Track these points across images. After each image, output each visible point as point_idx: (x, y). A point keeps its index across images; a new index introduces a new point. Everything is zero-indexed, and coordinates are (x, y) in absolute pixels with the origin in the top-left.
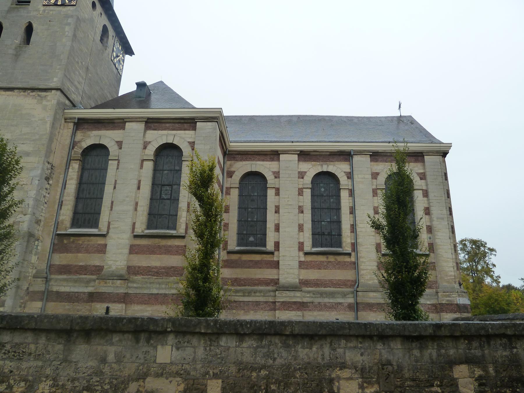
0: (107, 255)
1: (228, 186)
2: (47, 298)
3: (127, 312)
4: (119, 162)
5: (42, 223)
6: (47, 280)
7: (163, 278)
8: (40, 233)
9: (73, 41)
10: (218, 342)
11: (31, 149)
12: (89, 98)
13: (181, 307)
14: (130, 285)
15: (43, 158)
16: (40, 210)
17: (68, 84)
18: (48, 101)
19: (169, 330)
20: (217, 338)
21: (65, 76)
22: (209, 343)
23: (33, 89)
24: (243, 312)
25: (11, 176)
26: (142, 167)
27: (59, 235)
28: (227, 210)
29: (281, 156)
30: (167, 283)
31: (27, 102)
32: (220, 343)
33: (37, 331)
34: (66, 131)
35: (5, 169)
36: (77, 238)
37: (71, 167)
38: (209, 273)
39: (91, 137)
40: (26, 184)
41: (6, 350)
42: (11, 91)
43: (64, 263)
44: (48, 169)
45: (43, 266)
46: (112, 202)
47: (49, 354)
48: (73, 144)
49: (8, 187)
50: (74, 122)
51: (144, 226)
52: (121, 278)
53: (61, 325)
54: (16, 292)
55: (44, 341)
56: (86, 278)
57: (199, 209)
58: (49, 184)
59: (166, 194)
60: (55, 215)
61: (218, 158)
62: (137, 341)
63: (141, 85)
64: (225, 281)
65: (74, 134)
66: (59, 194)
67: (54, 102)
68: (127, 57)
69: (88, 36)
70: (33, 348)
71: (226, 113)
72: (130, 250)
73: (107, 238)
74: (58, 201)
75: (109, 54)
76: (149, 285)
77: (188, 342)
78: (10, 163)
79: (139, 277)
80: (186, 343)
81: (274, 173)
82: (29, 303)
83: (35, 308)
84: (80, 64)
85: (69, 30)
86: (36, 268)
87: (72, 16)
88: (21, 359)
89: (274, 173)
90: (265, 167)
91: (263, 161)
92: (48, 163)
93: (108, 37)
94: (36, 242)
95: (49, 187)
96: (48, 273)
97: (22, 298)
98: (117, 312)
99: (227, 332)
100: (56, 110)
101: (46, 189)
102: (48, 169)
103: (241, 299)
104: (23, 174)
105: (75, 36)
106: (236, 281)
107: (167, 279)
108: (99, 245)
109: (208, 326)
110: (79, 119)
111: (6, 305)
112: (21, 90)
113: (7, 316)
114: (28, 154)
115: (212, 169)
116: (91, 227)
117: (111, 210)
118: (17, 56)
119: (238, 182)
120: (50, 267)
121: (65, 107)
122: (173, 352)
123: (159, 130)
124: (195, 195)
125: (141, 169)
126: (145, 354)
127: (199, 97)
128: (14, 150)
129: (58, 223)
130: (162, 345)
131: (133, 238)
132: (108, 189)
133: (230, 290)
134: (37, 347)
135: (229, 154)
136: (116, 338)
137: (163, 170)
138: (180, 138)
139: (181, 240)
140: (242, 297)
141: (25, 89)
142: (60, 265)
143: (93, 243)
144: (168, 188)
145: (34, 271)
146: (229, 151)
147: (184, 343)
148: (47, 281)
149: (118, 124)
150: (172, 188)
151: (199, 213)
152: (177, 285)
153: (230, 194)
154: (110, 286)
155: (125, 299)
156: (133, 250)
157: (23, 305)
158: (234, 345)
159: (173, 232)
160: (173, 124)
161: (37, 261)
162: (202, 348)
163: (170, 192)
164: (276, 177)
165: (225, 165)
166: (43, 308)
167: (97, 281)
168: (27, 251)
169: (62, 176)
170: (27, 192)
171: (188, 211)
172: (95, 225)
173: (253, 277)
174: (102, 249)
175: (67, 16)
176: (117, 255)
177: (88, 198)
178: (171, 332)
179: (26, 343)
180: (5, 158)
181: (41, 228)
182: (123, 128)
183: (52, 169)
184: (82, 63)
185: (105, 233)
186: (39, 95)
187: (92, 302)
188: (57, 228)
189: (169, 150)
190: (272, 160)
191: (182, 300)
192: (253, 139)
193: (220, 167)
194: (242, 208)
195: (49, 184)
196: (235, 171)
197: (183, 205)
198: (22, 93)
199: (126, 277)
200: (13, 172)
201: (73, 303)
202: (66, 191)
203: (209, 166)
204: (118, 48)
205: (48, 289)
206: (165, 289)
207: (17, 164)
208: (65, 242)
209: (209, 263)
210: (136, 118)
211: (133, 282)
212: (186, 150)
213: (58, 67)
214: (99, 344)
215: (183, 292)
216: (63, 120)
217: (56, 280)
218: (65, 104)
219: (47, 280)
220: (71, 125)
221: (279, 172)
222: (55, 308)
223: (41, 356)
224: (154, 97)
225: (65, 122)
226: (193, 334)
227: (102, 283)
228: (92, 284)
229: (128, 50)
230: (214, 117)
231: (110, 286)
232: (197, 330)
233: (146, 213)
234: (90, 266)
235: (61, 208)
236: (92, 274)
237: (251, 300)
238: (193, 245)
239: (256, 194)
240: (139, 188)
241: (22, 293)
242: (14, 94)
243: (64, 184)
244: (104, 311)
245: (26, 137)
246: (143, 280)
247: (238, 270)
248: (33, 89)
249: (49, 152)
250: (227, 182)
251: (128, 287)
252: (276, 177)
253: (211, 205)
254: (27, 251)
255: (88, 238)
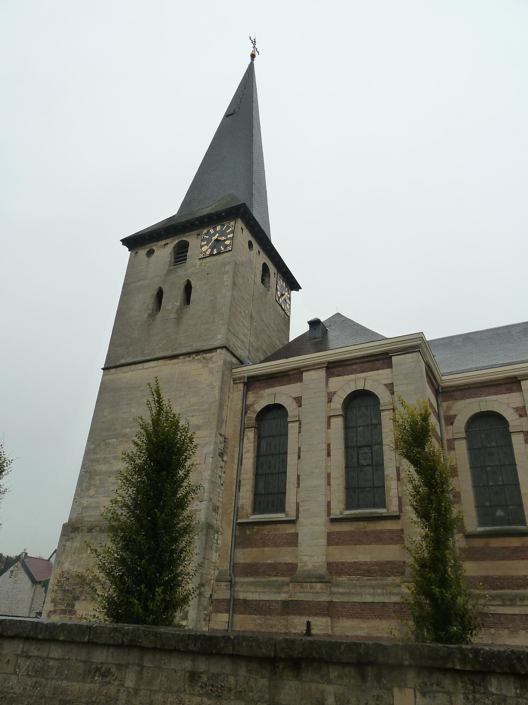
0: (300, 549)
1: (450, 437)
2: (233, 609)
3: (335, 629)
4: (300, 424)
5: (220, 511)
6: (232, 584)
7: (376, 580)
8: (219, 523)
9: (233, 289)
10: (486, 687)
11: (202, 421)
12: (257, 350)
13: (411, 623)
14: (334, 589)
15: (215, 430)
16: (217, 494)
17: (233, 339)
18: (214, 363)
19: (406, 663)
20: (483, 680)
21: (229, 330)
22: (471, 687)
23: (197, 353)
24: (506, 632)
25: (186, 456)
26: (329, 426)
27: (240, 524)
28: (454, 472)
29: (522, 383)
30: (384, 587)
31: (192, 368)
32: (490, 688)
33: (235, 658)
34: (235, 394)
35: (180, 449)
36: (261, 527)
37: (245, 438)
38: (446, 571)
39: (265, 398)
40: (200, 464)
41: (202, 683)
42: (176, 359)
43: (249, 560)
44: (221, 443)
45: (226, 566)
46: (298, 477)
47: (252, 691)
48: (246, 409)
49: (184, 470)
50: (244, 382)
51: (342, 506)
52: (321, 579)
53: (263, 650)
54: (199, 601)
55: (244, 673)
56: (277, 581)
57: (416, 476)
58: (223, 461)
59: (365, 459)
60: (234, 498)
61: (429, 400)
62: (364, 678)
63: (315, 324)
64: (473, 582)
65: (245, 397)
66: (235, 472)
67: (221, 362)
68: (293, 293)
69: (248, 280)
70: (232, 682)
71: (429, 337)
72: (328, 540)
73: (298, 524)
74: (235, 481)
75: (272, 295)
76: (359, 590)
77: (437, 685)
78: (184, 441)
79: (344, 579)
80: (435, 686)
81: (517, 409)
82: (213, 614)
83: (220, 621)
84: (243, 313)
85: (227, 279)
86: (218, 569)
87: (229, 263)
88: (220, 696)
89: (517, 409)
90: (502, 404)
91: (496, 394)
92: (221, 435)
93: (269, 276)
94: (216, 535)
95: (223, 465)
96: (232, 576)
97: (206, 608)
98: (321, 630)
99: (498, 671)
100: (223, 371)
101: (221, 467)
102: (221, 443)
103: (501, 610)
104: (198, 452)
105: (234, 283)
106: (490, 582)
107: (382, 580)
108: (288, 534)
109: (464, 658)
110: (249, 378)
111: (189, 618)
112: (186, 356)
113: (200, 636)
114: (198, 428)
115: (425, 418)
116: (277, 512)
117: (298, 486)
118: (179, 320)
119: (463, 430)
120: (233, 567)
121: (232, 367)
122: (417, 700)
123: (343, 376)
124: (407, 457)
125: (328, 429)
126: (377, 700)
127: (389, 324)
128: (187, 426)
129: (238, 509)
130: (400, 687)
131: (330, 524)
132: (291, 459)
133: (484, 597)
134: (237, 680)
135: (444, 393)
136: (334, 673)
137: (357, 427)
138: (373, 381)
139: (394, 521)
140: (502, 608)
141: (189, 354)
142: (244, 564)
143: (281, 532)
144: (366, 450)
145: (217, 573)
146: (442, 388)
147: (432, 685)
148: (231, 585)
149: (293, 376)
150: (372, 450)
151: (417, 483)
152: (398, 589)
153: (454, 449)
154: (308, 592)
155: (329, 610)
156: (332, 539)
157: (208, 619)
158: (513, 694)
159: (382, 511)
160: (361, 365)
161: (218, 560)
162: (462, 696)
163: (370, 455)
164: (521, 416)
165: (441, 408)
166: (230, 623)
167: (291, 585)
168: (207, 547)
169: (237, 449)
170: (201, 473)
171: (399, 479)
172: (281, 508)
173: (514, 573)
174: (293, 541)
175: (224, 264)
176: (312, 550)
177: (269, 474)
178: (410, 666)
179: (224, 674)
180: (179, 437)
181: (219, 517)
182: (301, 380)
183: (225, 441)
184: (245, 312)
185: (294, 518)
186: (204, 358)
187: (288, 614)
188: (237, 515)
189: (360, 399)
190: (510, 391)
191: (412, 614)
192: (474, 366)
193: (434, 412)
194: (477, 467)
195: (223, 461)
196: (456, 415)
197: (390, 470)
198: (187, 359)
199: (328, 578)
200: (188, 452)
201: (265, 615)
202: (243, 467)
203: (421, 415)
204: (282, 285)
205: (234, 597)
206: (383, 595)
207: (191, 442)
208: (248, 532)
209: (445, 556)
210: (314, 365)
211: (337, 585)
212: (384, 396)
213: (221, 322)
214: (313, 681)
215: (411, 600)
216: (232, 382)
217: (242, 584)
218: (232, 363)
219: (232, 584)
220: (241, 386)
221: (524, 407)
222: (247, 624)
223: (243, 694)
224: (332, 334)
225: (234, 383)
226: (445, 671)
227: (298, 589)
228: (285, 589)
229: (293, 285)
230: (415, 346)
231: (308, 592)
232: (449, 665)
233: (342, 487)
234: (280, 563)
235: (239, 490)
236: (284, 575)
237: (517, 613)
238: (416, 531)
239: (494, 444)
240: (329, 455)
241: (205, 602)
242: (179, 361)
243: (240, 459)
244: (304, 629)
245: (196, 407)
246: (351, 582)
247: (487, 564)
248: (197, 353)
249: (220, 422)
250: (447, 432)
251: (332, 593)
252: (521, 416)
253: (433, 469)
254: (207, 547)
255: (274, 526)
